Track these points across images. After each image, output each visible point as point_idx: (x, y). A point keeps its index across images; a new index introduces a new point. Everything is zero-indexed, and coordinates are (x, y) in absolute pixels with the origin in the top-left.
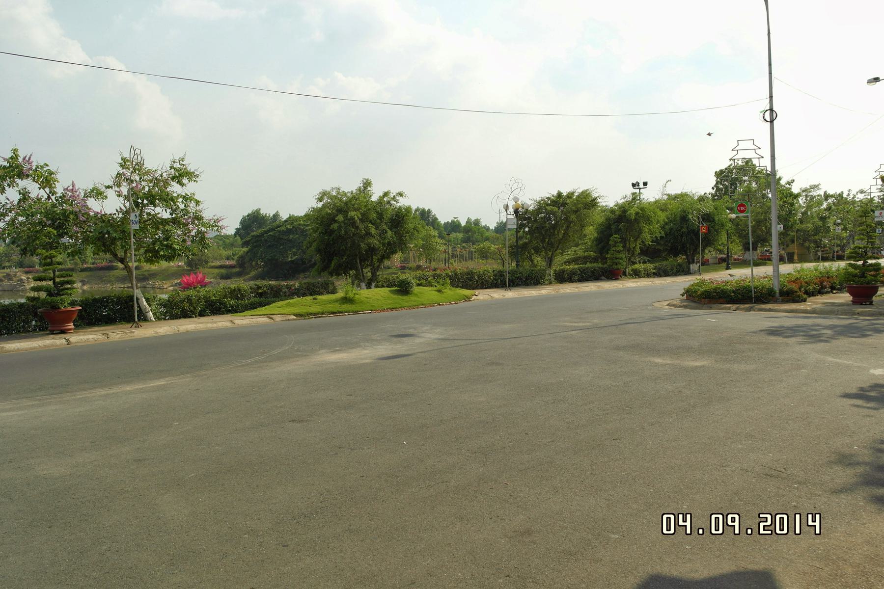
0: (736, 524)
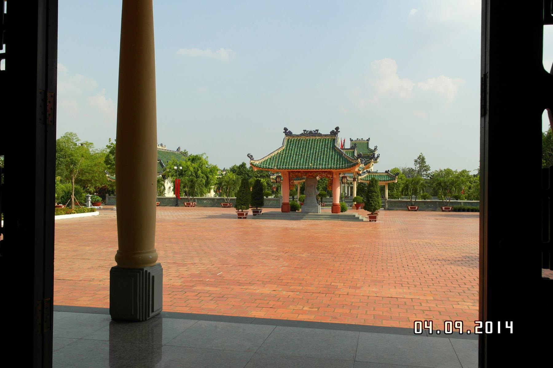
0: (461, 327)
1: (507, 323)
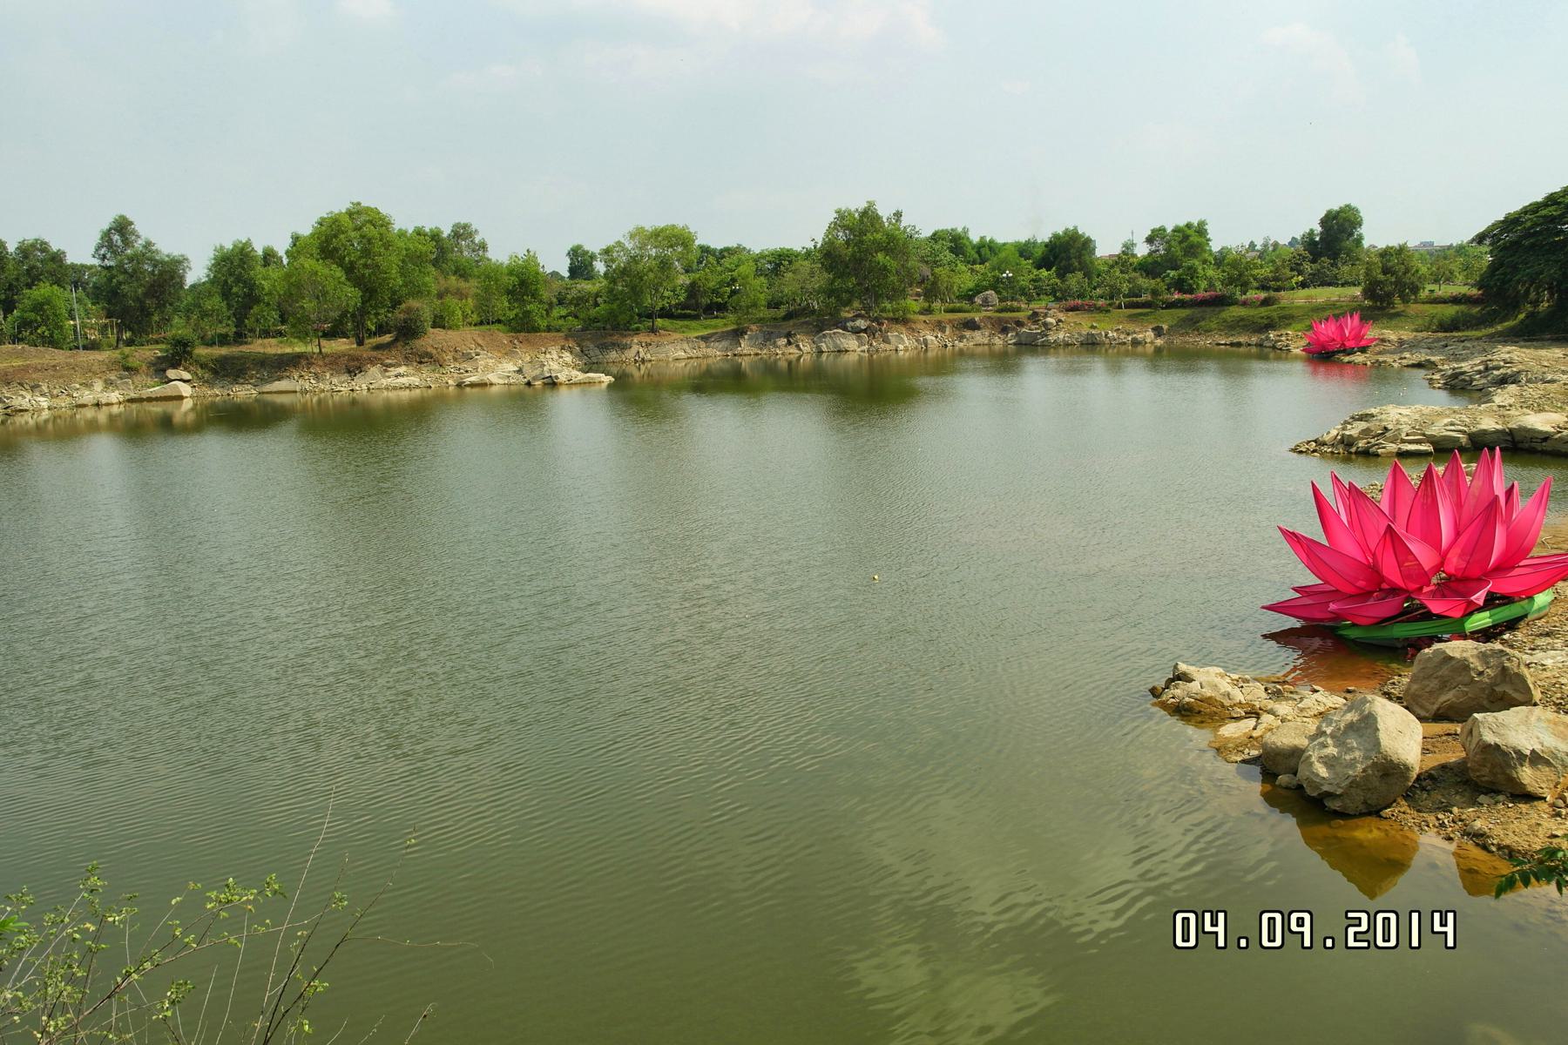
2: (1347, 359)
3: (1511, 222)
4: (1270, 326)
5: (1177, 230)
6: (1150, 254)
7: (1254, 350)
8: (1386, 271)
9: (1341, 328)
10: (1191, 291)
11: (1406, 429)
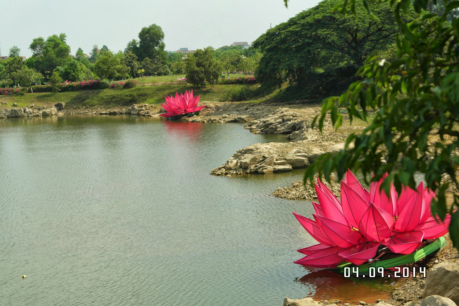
1: (421, 268)
2: (190, 119)
3: (270, 35)
4: (133, 101)
5: (50, 40)
6: (35, 55)
7: (124, 117)
8: (199, 65)
9: (184, 100)
10: (74, 80)
11: (276, 156)
